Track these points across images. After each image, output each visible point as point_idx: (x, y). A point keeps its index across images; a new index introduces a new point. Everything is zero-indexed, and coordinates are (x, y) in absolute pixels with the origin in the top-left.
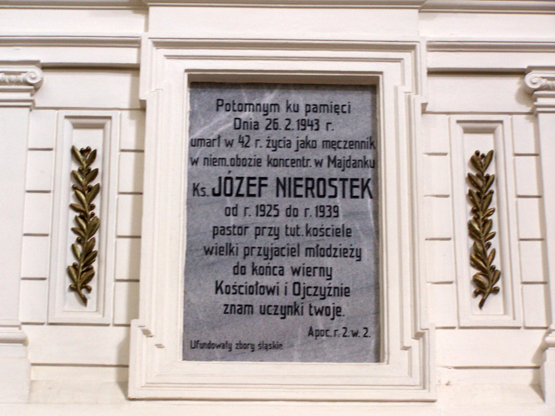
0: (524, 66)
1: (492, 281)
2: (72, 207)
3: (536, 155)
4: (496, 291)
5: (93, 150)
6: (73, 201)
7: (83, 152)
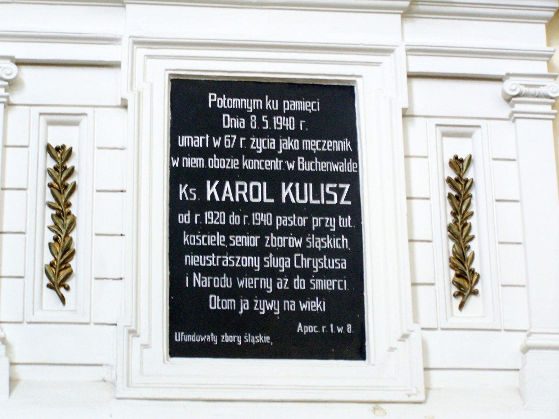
0: (500, 72)
1: (471, 282)
2: (50, 206)
3: (6, 146)
4: (476, 293)
5: (67, 148)
6: (51, 199)
7: (57, 149)
